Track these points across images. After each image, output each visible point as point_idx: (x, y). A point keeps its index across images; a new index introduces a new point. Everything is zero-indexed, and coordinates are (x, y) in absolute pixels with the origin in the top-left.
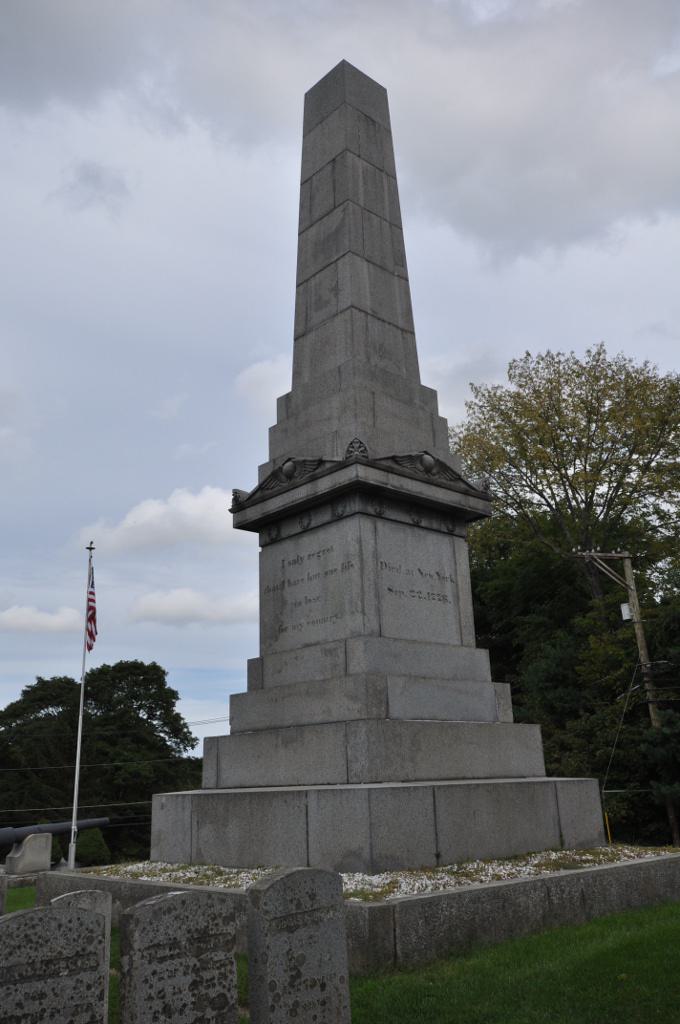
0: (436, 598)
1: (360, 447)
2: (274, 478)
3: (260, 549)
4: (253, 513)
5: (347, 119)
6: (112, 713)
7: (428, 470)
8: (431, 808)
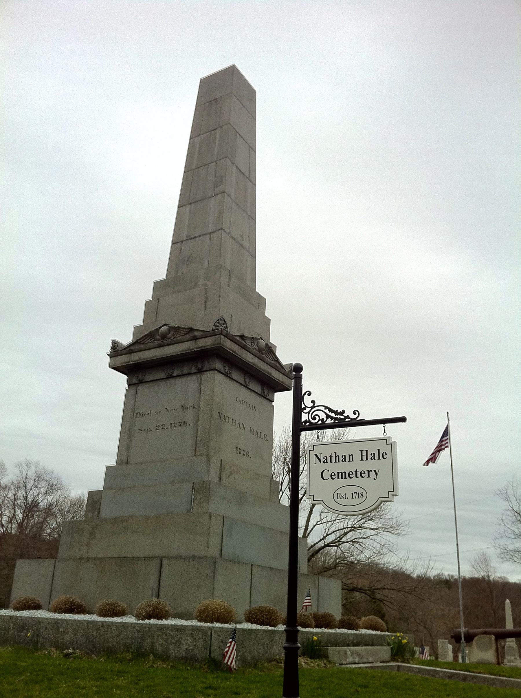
0: (242, 452)
1: (224, 324)
2: (144, 338)
3: (127, 386)
4: (122, 360)
5: (224, 113)
6: (398, 634)
7: (260, 350)
8: (51, 574)
